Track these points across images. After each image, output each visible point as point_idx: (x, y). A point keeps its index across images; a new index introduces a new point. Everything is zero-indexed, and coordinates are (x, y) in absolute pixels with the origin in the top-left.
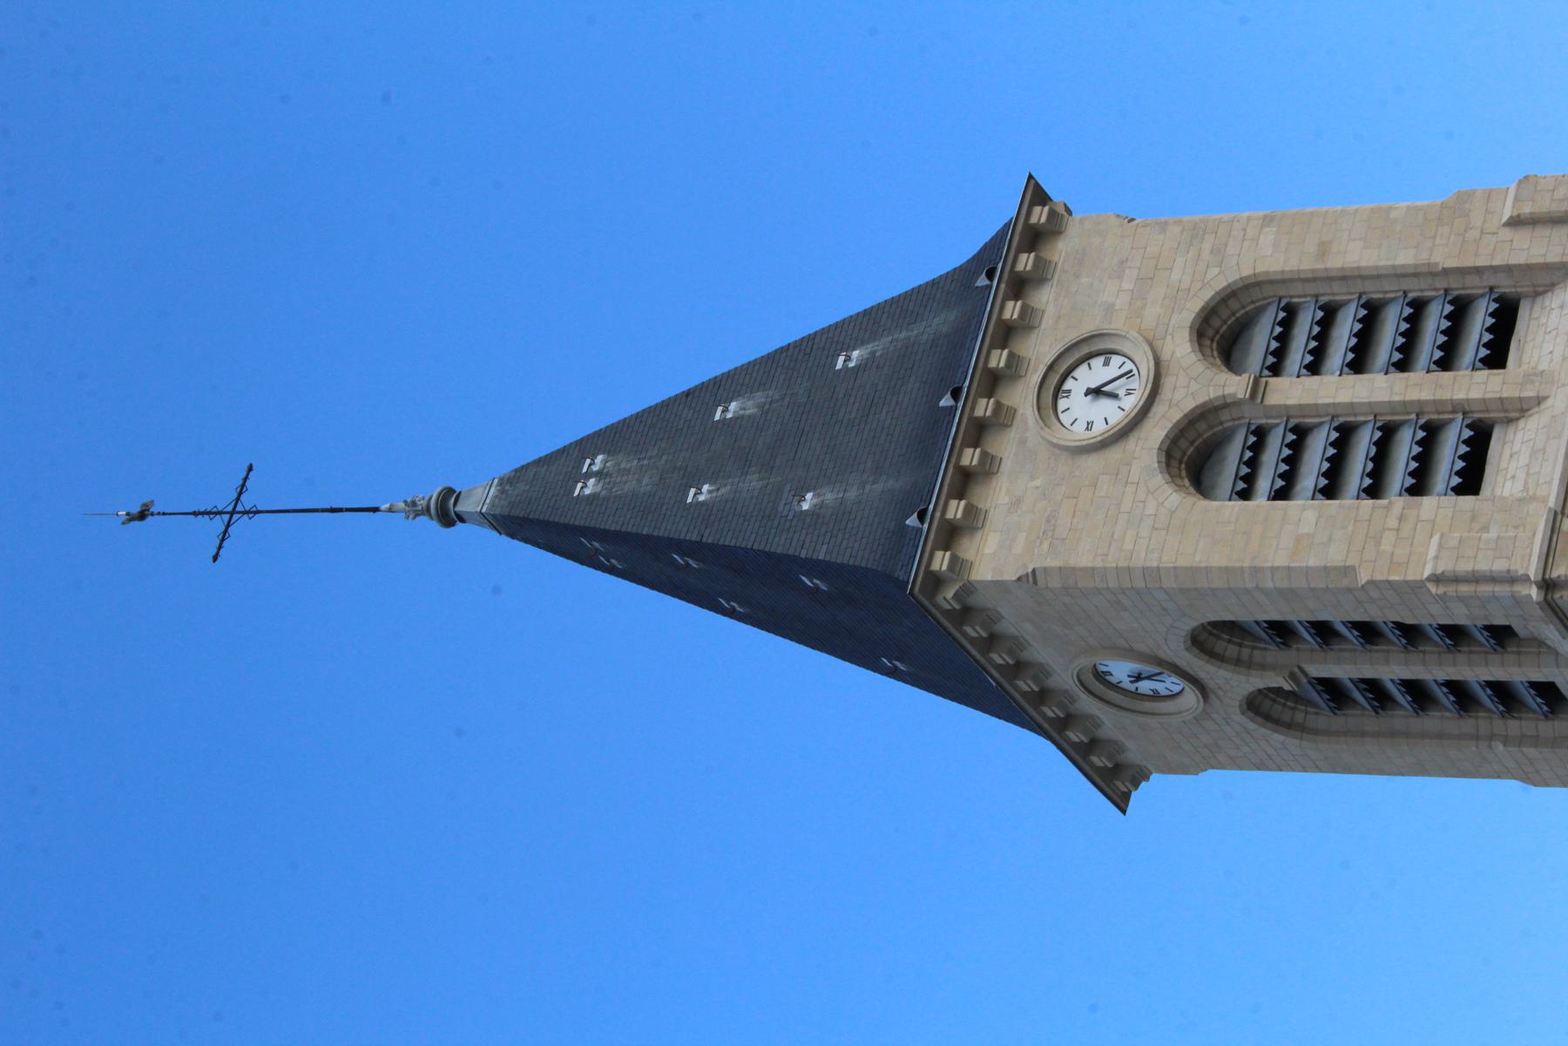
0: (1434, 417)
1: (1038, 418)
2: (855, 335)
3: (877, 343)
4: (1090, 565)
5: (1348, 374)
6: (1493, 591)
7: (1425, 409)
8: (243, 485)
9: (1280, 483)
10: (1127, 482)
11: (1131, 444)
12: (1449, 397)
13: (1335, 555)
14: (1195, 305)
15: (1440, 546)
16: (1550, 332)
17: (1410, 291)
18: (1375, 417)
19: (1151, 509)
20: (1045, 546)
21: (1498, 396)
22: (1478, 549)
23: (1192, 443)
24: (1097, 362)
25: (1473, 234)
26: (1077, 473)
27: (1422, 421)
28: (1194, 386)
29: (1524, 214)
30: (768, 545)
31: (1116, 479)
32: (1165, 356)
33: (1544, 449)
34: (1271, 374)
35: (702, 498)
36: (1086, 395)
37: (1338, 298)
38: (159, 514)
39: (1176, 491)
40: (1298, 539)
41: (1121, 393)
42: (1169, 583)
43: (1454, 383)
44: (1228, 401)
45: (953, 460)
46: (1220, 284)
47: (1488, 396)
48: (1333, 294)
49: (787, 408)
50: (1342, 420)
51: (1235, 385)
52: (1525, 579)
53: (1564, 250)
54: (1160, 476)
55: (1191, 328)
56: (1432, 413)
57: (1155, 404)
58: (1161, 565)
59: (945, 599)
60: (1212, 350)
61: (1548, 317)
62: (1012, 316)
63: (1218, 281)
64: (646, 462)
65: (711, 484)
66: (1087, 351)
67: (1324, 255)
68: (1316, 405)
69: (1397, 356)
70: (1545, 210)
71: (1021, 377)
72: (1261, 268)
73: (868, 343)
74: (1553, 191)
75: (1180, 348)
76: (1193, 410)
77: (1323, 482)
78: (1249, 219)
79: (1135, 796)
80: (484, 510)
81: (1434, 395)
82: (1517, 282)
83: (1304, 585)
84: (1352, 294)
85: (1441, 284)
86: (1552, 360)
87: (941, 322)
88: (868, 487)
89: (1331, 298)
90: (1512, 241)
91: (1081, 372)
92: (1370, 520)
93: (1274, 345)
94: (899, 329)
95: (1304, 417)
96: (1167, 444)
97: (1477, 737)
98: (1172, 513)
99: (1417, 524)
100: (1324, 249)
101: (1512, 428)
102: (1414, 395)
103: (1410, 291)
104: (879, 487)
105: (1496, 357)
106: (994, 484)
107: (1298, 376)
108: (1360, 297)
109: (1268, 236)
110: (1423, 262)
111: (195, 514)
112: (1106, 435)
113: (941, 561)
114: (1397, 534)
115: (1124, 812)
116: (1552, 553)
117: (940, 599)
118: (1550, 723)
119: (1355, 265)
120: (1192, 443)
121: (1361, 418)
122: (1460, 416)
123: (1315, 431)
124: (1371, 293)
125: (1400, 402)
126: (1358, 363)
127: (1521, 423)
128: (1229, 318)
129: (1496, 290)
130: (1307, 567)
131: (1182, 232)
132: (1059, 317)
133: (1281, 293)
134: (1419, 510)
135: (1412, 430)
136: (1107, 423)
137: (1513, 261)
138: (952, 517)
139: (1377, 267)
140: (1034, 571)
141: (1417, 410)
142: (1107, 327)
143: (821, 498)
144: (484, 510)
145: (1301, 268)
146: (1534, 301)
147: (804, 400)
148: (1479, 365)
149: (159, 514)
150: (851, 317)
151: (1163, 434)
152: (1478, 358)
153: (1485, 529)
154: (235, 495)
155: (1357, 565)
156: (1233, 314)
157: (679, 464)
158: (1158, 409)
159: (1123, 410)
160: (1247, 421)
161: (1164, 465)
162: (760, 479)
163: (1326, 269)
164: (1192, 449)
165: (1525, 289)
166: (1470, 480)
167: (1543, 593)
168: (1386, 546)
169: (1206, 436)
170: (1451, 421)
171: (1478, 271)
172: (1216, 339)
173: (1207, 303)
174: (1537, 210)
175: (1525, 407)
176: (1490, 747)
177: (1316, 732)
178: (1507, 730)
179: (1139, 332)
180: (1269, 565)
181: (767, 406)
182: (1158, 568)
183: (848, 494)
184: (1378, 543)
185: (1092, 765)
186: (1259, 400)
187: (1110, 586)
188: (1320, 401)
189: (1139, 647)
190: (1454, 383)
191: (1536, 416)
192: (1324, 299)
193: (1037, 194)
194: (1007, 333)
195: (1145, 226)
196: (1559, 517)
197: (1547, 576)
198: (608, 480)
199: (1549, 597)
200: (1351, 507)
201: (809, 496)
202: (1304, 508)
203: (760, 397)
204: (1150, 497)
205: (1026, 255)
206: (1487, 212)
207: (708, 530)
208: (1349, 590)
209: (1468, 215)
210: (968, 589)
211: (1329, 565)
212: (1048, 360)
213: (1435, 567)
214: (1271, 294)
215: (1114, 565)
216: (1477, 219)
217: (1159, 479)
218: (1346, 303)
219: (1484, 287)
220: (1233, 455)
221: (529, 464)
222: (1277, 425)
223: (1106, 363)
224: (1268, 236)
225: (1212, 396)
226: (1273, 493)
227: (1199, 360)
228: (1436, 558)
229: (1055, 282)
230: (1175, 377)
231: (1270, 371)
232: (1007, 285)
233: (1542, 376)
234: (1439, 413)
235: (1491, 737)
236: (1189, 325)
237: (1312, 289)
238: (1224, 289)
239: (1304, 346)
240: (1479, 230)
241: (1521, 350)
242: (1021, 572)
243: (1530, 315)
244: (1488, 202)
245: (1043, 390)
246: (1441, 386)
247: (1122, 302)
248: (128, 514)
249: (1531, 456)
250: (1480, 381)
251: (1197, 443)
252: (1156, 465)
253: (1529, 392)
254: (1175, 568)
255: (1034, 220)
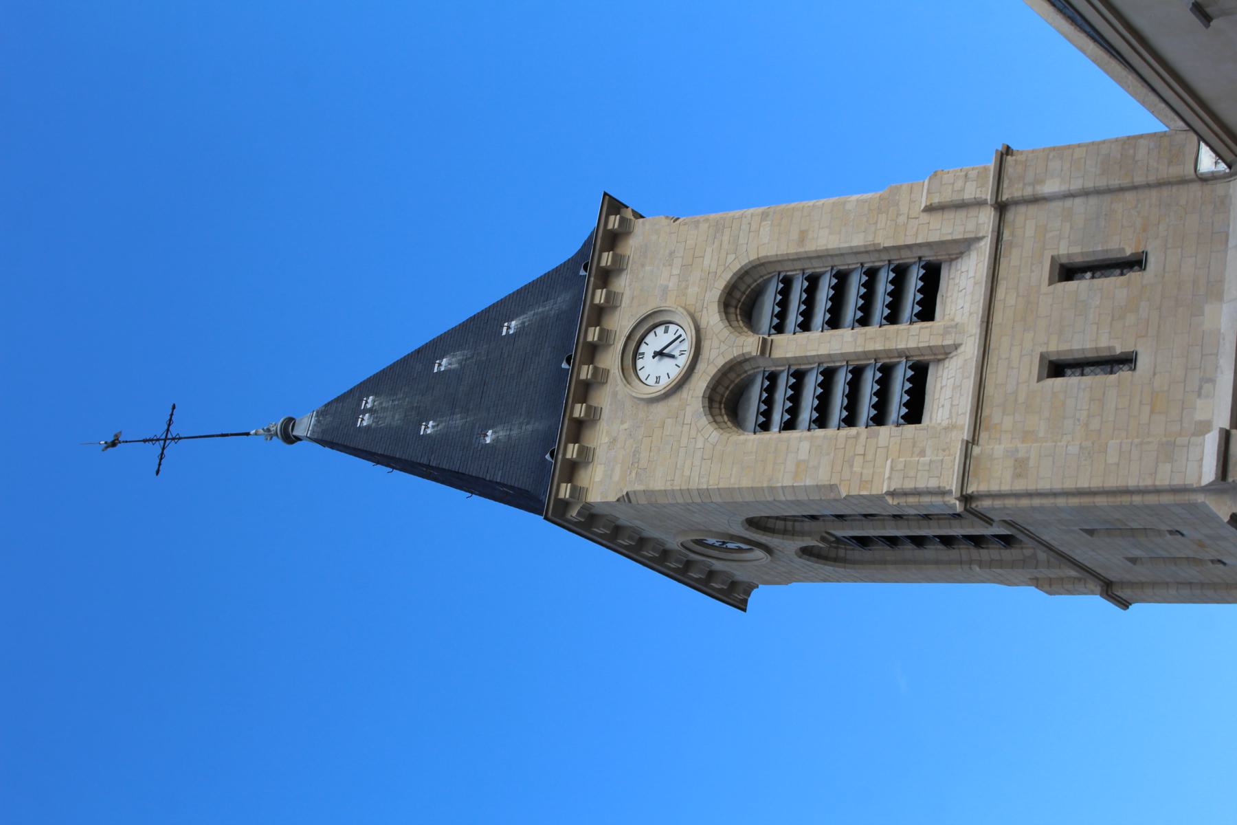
0: (887, 361)
1: (622, 377)
2: (496, 322)
3: (525, 316)
4: (663, 488)
5: (827, 330)
6: (931, 502)
7: (880, 356)
8: (170, 420)
9: (787, 417)
10: (683, 424)
11: (685, 393)
12: (894, 348)
13: (823, 476)
14: (721, 284)
15: (892, 469)
16: (961, 291)
17: (865, 263)
18: (847, 362)
19: (700, 444)
20: (633, 474)
21: (927, 345)
22: (918, 470)
23: (727, 388)
24: (660, 330)
25: (902, 219)
26: (651, 418)
27: (879, 365)
28: (724, 347)
29: (935, 203)
30: (467, 470)
31: (676, 421)
32: (703, 324)
33: (960, 386)
34: (775, 332)
35: (429, 431)
36: (654, 357)
37: (818, 270)
38: (123, 442)
39: (716, 429)
40: (798, 463)
41: (676, 353)
42: (717, 499)
43: (897, 336)
44: (747, 357)
45: (568, 415)
46: (736, 267)
47: (921, 345)
48: (814, 268)
49: (475, 365)
50: (825, 365)
51: (749, 344)
52: (950, 492)
53: (965, 229)
54: (705, 418)
55: (719, 301)
56: (885, 358)
57: (699, 362)
58: (709, 487)
59: (571, 516)
60: (736, 315)
61: (960, 278)
62: (600, 301)
63: (735, 265)
64: (396, 403)
65: (434, 421)
66: (652, 323)
67: (803, 240)
68: (806, 357)
69: (859, 314)
70: (949, 200)
71: (611, 345)
72: (763, 253)
73: (520, 316)
74: (953, 184)
75: (712, 318)
76: (723, 366)
77: (815, 415)
78: (752, 215)
79: (750, 600)
80: (308, 435)
81: (884, 346)
82: (937, 253)
83: (806, 498)
84: (826, 267)
85: (885, 257)
86: (963, 314)
87: (562, 301)
88: (524, 428)
89: (813, 270)
90: (929, 223)
91: (650, 338)
92: (845, 448)
93: (777, 309)
94: (538, 305)
95: (800, 364)
96: (708, 393)
97: (961, 562)
98: (714, 446)
99: (876, 450)
100: (802, 239)
101: (941, 366)
102: (871, 347)
103: (865, 263)
104: (530, 427)
105: (927, 312)
106: (598, 427)
107: (794, 333)
108: (832, 269)
109: (766, 228)
110: (869, 243)
111: (145, 441)
112: (667, 389)
113: (565, 491)
114: (864, 459)
115: (744, 610)
116: (967, 475)
117: (568, 516)
118: (1008, 551)
119: (825, 248)
120: (727, 388)
121: (838, 364)
122: (904, 360)
123: (809, 374)
124: (839, 265)
125: (862, 352)
126: (834, 322)
127: (947, 362)
128: (746, 290)
129: (923, 259)
130: (805, 486)
131: (709, 228)
132: (633, 298)
133: (781, 269)
134: (878, 438)
135: (872, 372)
136: (679, 367)
137: (931, 239)
138: (570, 457)
139: (839, 248)
140: (627, 493)
141: (875, 357)
142: (665, 305)
143: (497, 435)
144: (308, 435)
145: (789, 252)
146: (950, 265)
147: (484, 358)
148: (915, 319)
149: (123, 442)
150: (510, 295)
151: (705, 385)
152: (914, 313)
153: (922, 453)
154: (166, 427)
155: (838, 483)
156: (749, 286)
157: (415, 405)
158: (701, 366)
159: (679, 367)
160: (763, 369)
161: (707, 408)
162: (462, 418)
163: (806, 252)
164: (728, 392)
165: (943, 257)
166: (914, 414)
167: (963, 505)
168: (857, 469)
169: (736, 381)
170: (899, 363)
171: (909, 247)
172: (739, 306)
173: (729, 282)
174: (943, 200)
175: (948, 351)
176: (971, 568)
177: (854, 562)
178: (980, 557)
179: (685, 308)
180: (779, 485)
181: (463, 363)
182: (708, 489)
183: (512, 433)
184: (851, 466)
185: (714, 589)
186: (767, 355)
187: (679, 501)
188: (809, 354)
189: (714, 529)
190: (897, 336)
191: (955, 358)
192: (808, 272)
193: (613, 205)
194: (599, 314)
195: (685, 224)
196: (970, 445)
197: (964, 493)
198: (375, 415)
199: (968, 507)
200: (833, 434)
201: (490, 432)
202: (800, 440)
203: (459, 355)
204: (699, 434)
205: (607, 253)
206: (911, 201)
207: (433, 456)
208: (836, 500)
209: (898, 205)
210: (587, 507)
211: (819, 484)
212: (626, 332)
213: (889, 486)
214: (773, 270)
215: (678, 488)
216: (904, 209)
217: (704, 420)
218: (824, 273)
219: (915, 258)
220: (755, 393)
221: (332, 401)
222: (783, 371)
223: (666, 331)
224: (766, 228)
225: (735, 355)
226: (783, 425)
227: (726, 327)
228: (890, 478)
229: (629, 271)
230: (710, 341)
231: (775, 330)
232: (595, 278)
233: (956, 328)
234: (890, 358)
235: (971, 562)
236: (717, 300)
237: (799, 265)
238: (740, 270)
239: (797, 309)
240: (906, 216)
241: (944, 304)
242: (619, 495)
243: (949, 276)
244: (911, 193)
245: (625, 355)
246: (888, 339)
247: (672, 284)
248: (106, 443)
249: (953, 390)
250: (914, 334)
251: (730, 388)
252: (702, 409)
253: (948, 341)
254: (718, 489)
255: (610, 226)
